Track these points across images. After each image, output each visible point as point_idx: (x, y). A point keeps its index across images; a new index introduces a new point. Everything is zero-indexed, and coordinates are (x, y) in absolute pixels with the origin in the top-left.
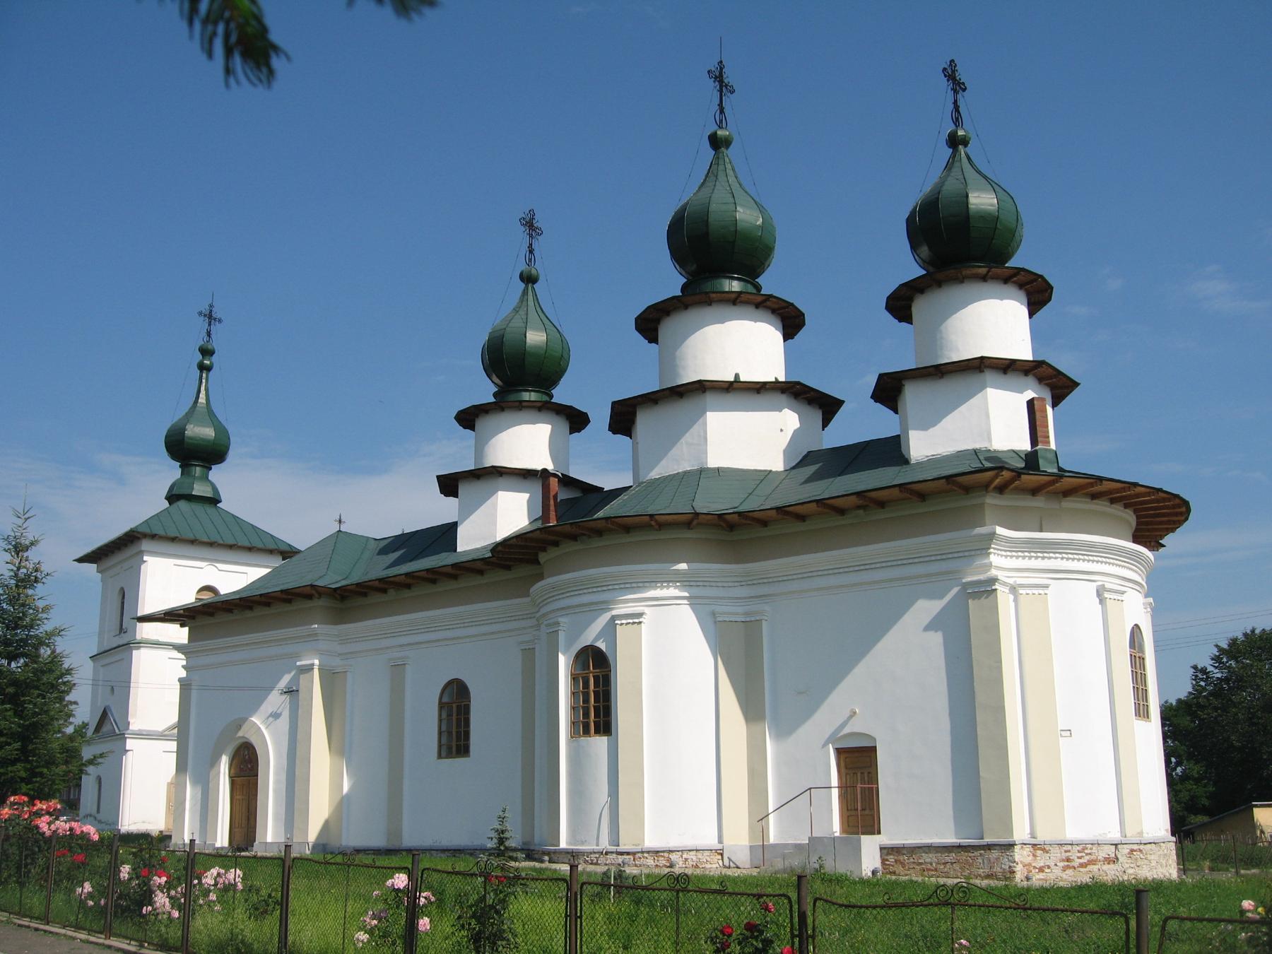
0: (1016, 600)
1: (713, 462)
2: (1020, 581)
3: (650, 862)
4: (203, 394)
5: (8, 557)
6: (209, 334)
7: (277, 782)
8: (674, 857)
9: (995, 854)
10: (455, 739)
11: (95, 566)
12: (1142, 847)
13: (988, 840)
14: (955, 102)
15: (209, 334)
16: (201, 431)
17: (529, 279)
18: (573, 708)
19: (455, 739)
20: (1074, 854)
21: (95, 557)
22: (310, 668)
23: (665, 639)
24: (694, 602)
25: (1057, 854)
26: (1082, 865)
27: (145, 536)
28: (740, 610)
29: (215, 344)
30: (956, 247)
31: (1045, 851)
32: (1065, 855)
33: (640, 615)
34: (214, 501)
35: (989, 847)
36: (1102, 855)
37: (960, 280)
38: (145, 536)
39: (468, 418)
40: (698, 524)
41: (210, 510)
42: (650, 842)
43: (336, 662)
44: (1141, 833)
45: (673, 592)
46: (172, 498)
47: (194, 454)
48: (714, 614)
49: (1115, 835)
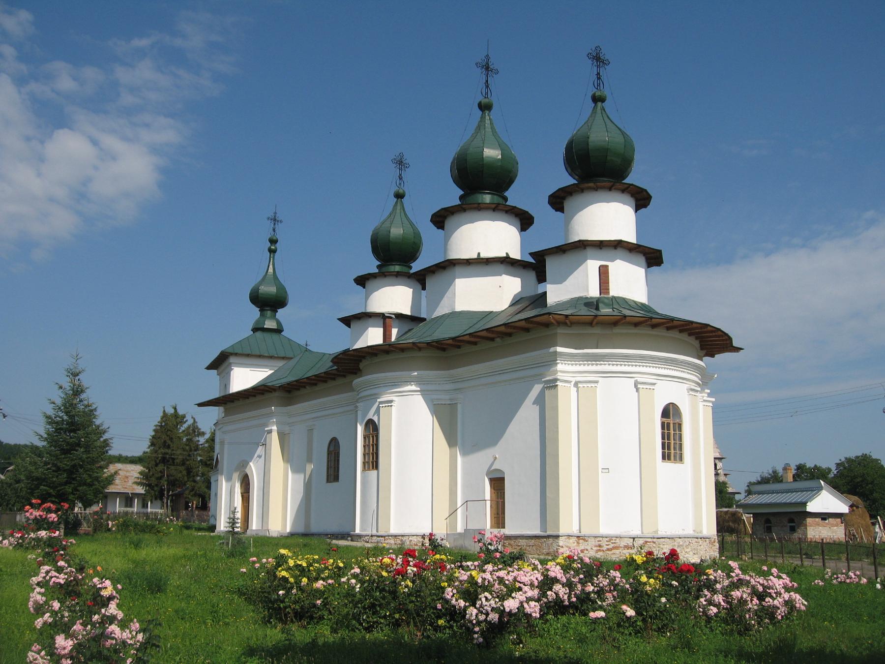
0: (577, 391)
1: (459, 308)
2: (578, 379)
3: (392, 541)
4: (271, 266)
5: (68, 379)
6: (274, 230)
7: (258, 496)
8: (404, 539)
9: (551, 540)
10: (671, 448)
11: (216, 371)
12: (655, 540)
13: (549, 533)
14: (598, 74)
15: (274, 230)
16: (269, 289)
17: (399, 196)
18: (364, 455)
19: (671, 448)
20: (604, 542)
21: (211, 367)
22: (270, 432)
23: (407, 415)
24: (423, 393)
25: (592, 542)
26: (608, 550)
27: (232, 354)
28: (447, 397)
29: (279, 236)
30: (596, 169)
31: (584, 540)
32: (597, 543)
33: (391, 401)
34: (279, 331)
35: (548, 537)
36: (623, 544)
37: (596, 189)
38: (232, 354)
39: (362, 281)
40: (597, 323)
41: (275, 336)
42: (393, 530)
43: (287, 429)
44: (656, 532)
45: (414, 388)
46: (255, 330)
47: (269, 303)
48: (432, 400)
49: (637, 532)
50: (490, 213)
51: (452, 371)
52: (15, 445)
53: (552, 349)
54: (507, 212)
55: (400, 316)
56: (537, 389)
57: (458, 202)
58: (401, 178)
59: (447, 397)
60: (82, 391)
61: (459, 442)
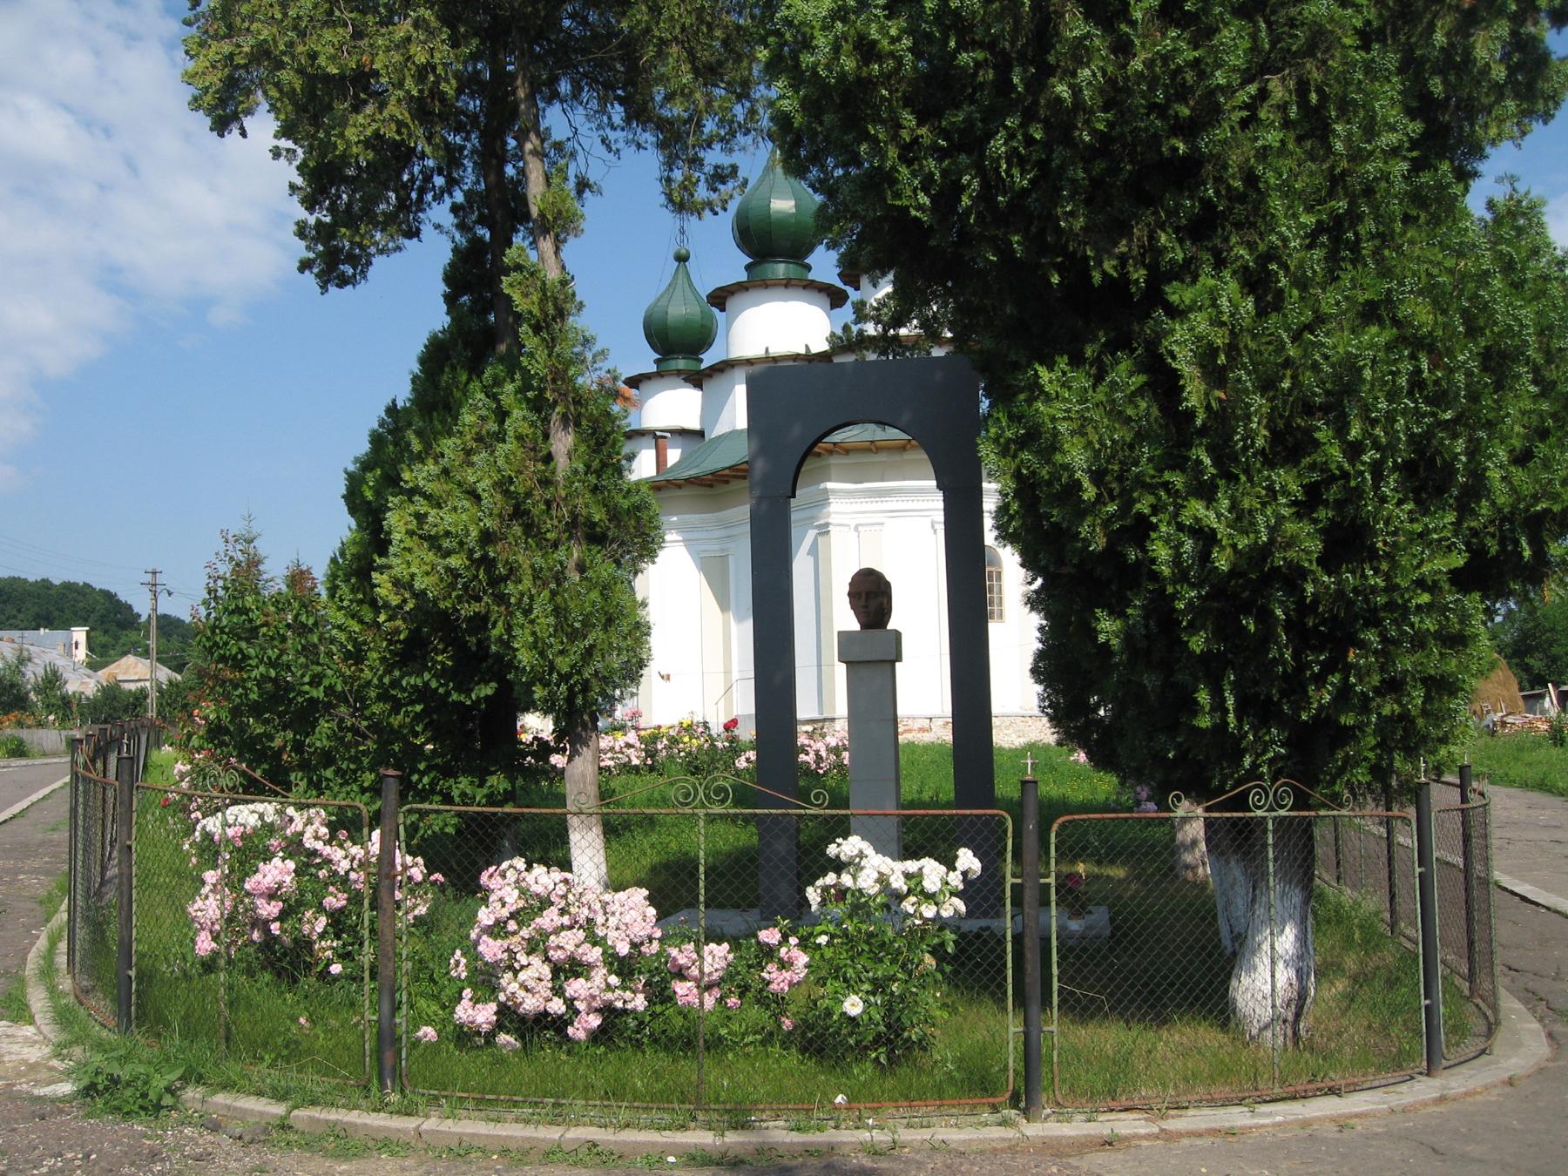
13: (826, 715)
17: (682, 259)
28: (716, 547)
35: (825, 720)
50: (781, 291)
51: (721, 514)
52: (69, 587)
53: (822, 486)
54: (804, 287)
55: (683, 433)
56: (812, 534)
57: (743, 276)
58: (682, 232)
59: (716, 547)
60: (259, 562)
61: (733, 604)
